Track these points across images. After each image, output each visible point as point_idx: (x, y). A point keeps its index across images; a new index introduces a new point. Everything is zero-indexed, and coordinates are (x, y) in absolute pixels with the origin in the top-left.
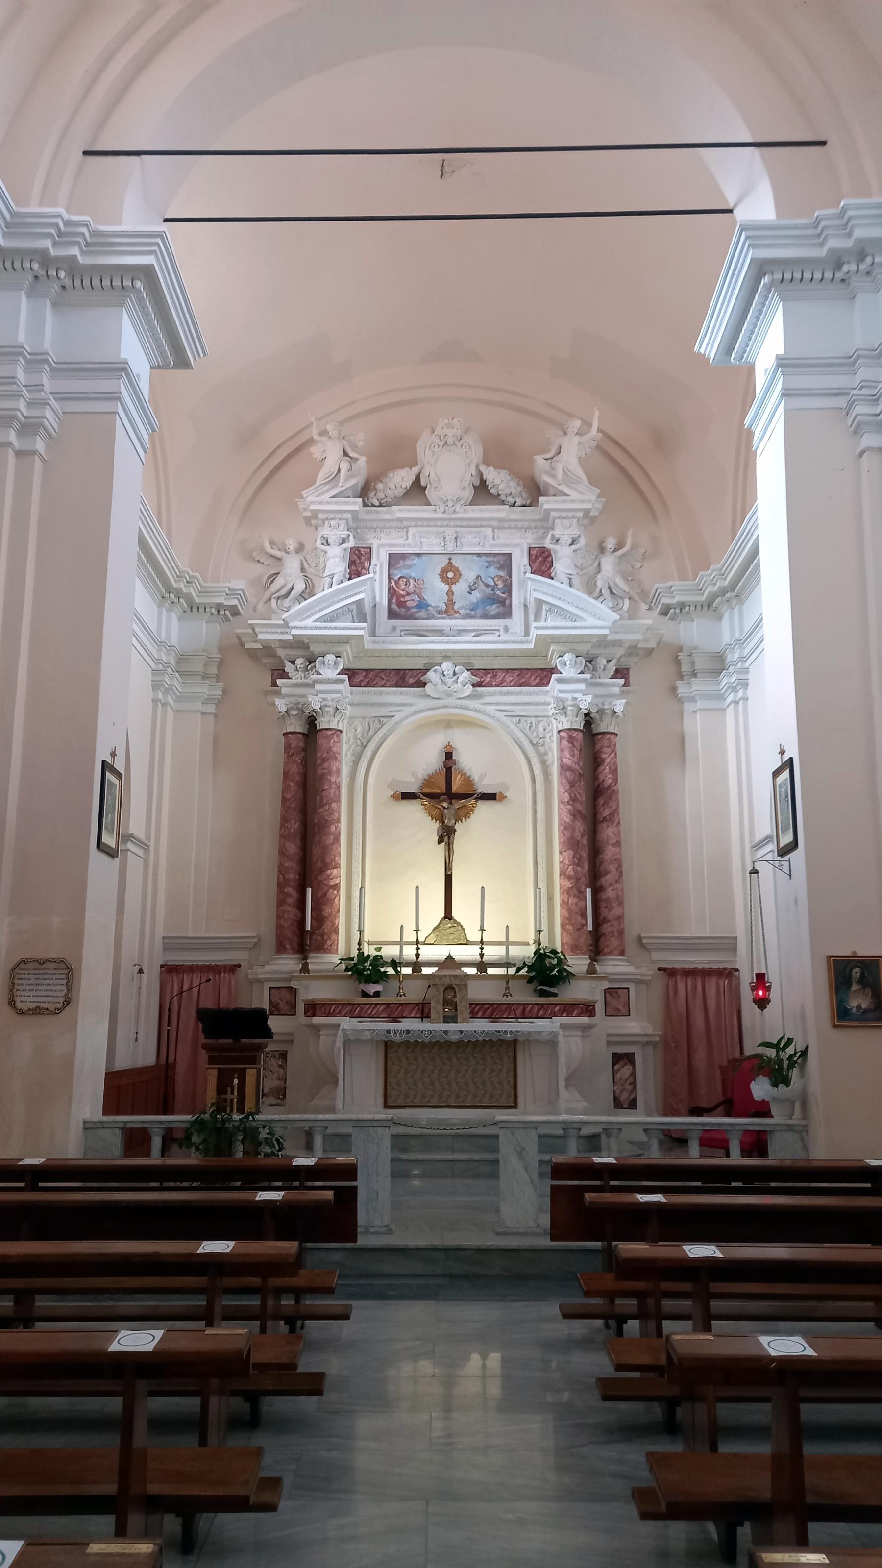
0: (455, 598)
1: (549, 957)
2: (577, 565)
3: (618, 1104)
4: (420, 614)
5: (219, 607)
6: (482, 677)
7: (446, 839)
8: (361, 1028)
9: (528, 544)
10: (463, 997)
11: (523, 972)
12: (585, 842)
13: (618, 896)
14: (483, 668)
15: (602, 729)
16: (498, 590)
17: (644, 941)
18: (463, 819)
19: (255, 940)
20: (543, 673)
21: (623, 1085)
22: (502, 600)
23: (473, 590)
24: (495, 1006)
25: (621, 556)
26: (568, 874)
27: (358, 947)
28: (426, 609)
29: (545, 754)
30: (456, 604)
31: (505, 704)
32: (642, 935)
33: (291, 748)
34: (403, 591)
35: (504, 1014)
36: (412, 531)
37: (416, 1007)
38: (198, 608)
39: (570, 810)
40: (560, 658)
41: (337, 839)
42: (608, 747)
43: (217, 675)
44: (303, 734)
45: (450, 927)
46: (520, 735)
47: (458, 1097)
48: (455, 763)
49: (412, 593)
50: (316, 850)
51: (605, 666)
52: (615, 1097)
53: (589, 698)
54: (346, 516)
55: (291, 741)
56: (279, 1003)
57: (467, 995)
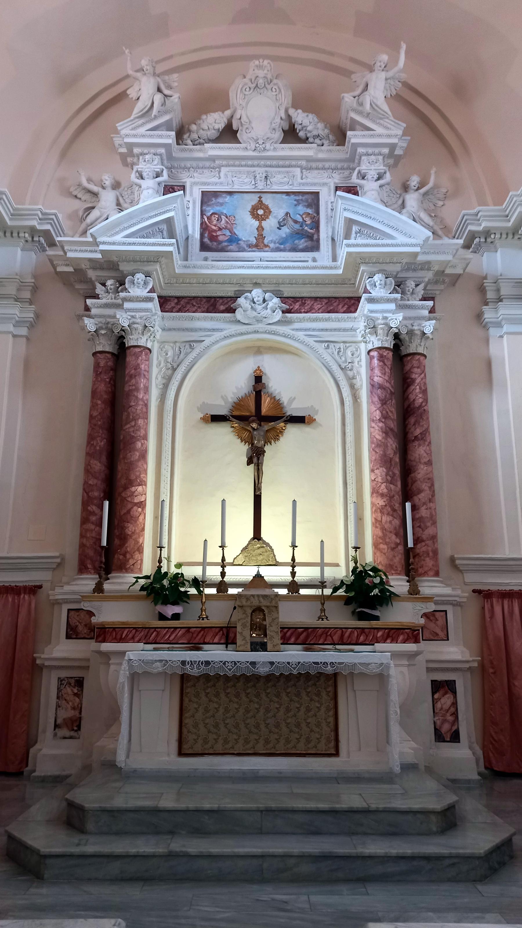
0: (265, 233)
1: (370, 576)
2: (383, 199)
3: (439, 737)
4: (231, 247)
5: (33, 231)
6: (291, 305)
7: (255, 460)
8: (150, 658)
9: (335, 183)
10: (273, 620)
11: (341, 592)
12: (397, 460)
13: (431, 514)
14: (292, 296)
15: (412, 350)
16: (307, 225)
17: (458, 562)
18: (272, 441)
19: (58, 560)
20: (350, 302)
21: (444, 716)
22: (310, 235)
23: (283, 226)
24: (310, 630)
25: (425, 194)
26: (381, 492)
27: (158, 564)
28: (238, 244)
29: (354, 378)
30: (265, 239)
31: (314, 330)
32: (456, 556)
33: (99, 367)
34: (215, 226)
35: (319, 641)
36: (224, 170)
37: (219, 631)
38: (12, 233)
39: (382, 428)
40: (370, 279)
41: (144, 456)
42: (418, 367)
43: (30, 299)
44: (112, 354)
45: (259, 548)
46: (328, 358)
47: (267, 742)
48: (264, 386)
49: (223, 228)
50: (121, 467)
51: (413, 290)
52: (436, 729)
53: (400, 316)
54: (160, 150)
55: (100, 360)
56: (77, 626)
57: (278, 618)
